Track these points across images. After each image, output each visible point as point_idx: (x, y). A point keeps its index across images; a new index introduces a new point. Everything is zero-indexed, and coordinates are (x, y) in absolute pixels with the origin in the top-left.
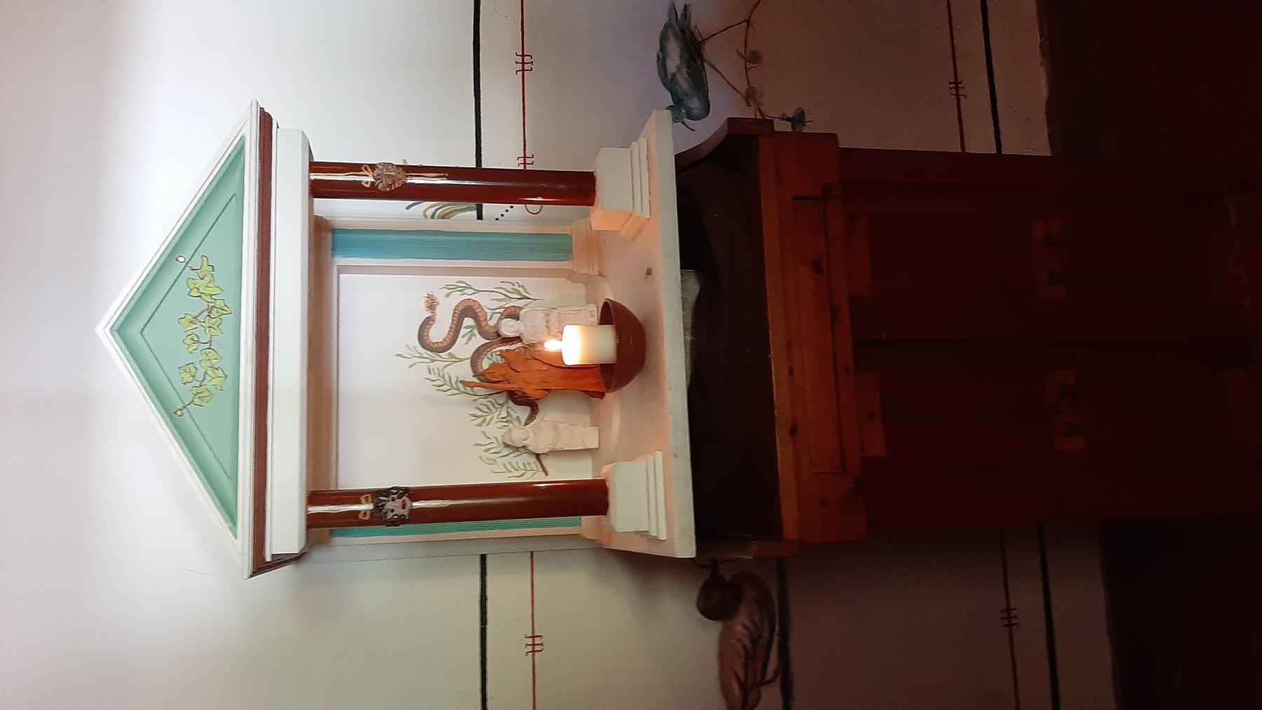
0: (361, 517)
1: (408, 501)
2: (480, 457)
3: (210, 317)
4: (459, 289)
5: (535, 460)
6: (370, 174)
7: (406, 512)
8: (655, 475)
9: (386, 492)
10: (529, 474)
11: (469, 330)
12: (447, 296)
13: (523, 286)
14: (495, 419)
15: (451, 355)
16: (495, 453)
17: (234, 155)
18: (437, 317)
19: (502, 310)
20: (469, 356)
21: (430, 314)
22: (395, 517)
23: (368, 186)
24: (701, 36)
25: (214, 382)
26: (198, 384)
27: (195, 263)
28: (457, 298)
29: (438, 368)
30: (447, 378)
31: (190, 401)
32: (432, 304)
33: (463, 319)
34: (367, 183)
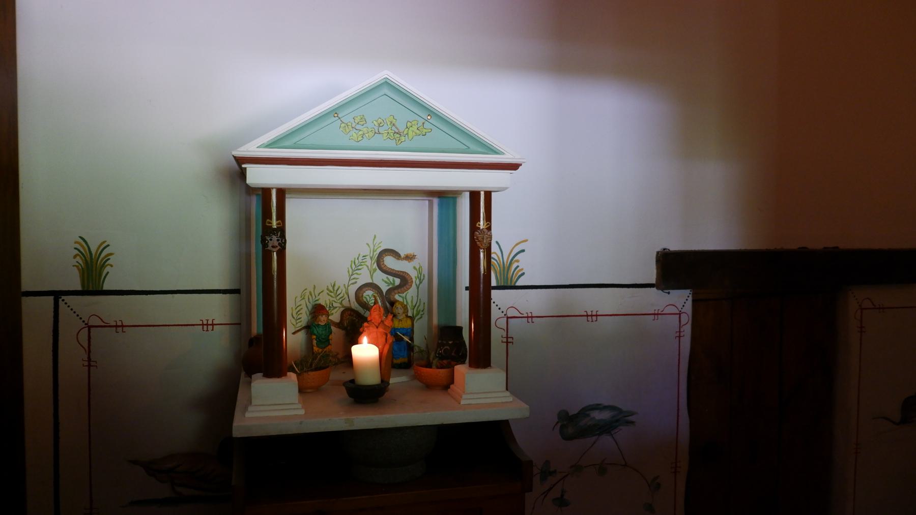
0: (268, 220)
1: (277, 249)
2: (306, 289)
3: (394, 133)
4: (419, 275)
5: (303, 326)
6: (484, 227)
7: (270, 248)
8: (276, 410)
9: (283, 236)
10: (294, 321)
11: (392, 282)
12: (415, 268)
13: (421, 317)
14: (332, 299)
15: (375, 270)
16: (309, 298)
17: (493, 148)
18: (400, 261)
19: (405, 303)
20: (375, 282)
21: (402, 257)
22: (267, 242)
23: (477, 226)
24: (615, 433)
25: (354, 135)
26: (353, 126)
27: (427, 125)
28: (413, 274)
29: (366, 262)
30: (360, 267)
31: (343, 121)
32: (409, 258)
33: (399, 278)
34: (479, 225)
